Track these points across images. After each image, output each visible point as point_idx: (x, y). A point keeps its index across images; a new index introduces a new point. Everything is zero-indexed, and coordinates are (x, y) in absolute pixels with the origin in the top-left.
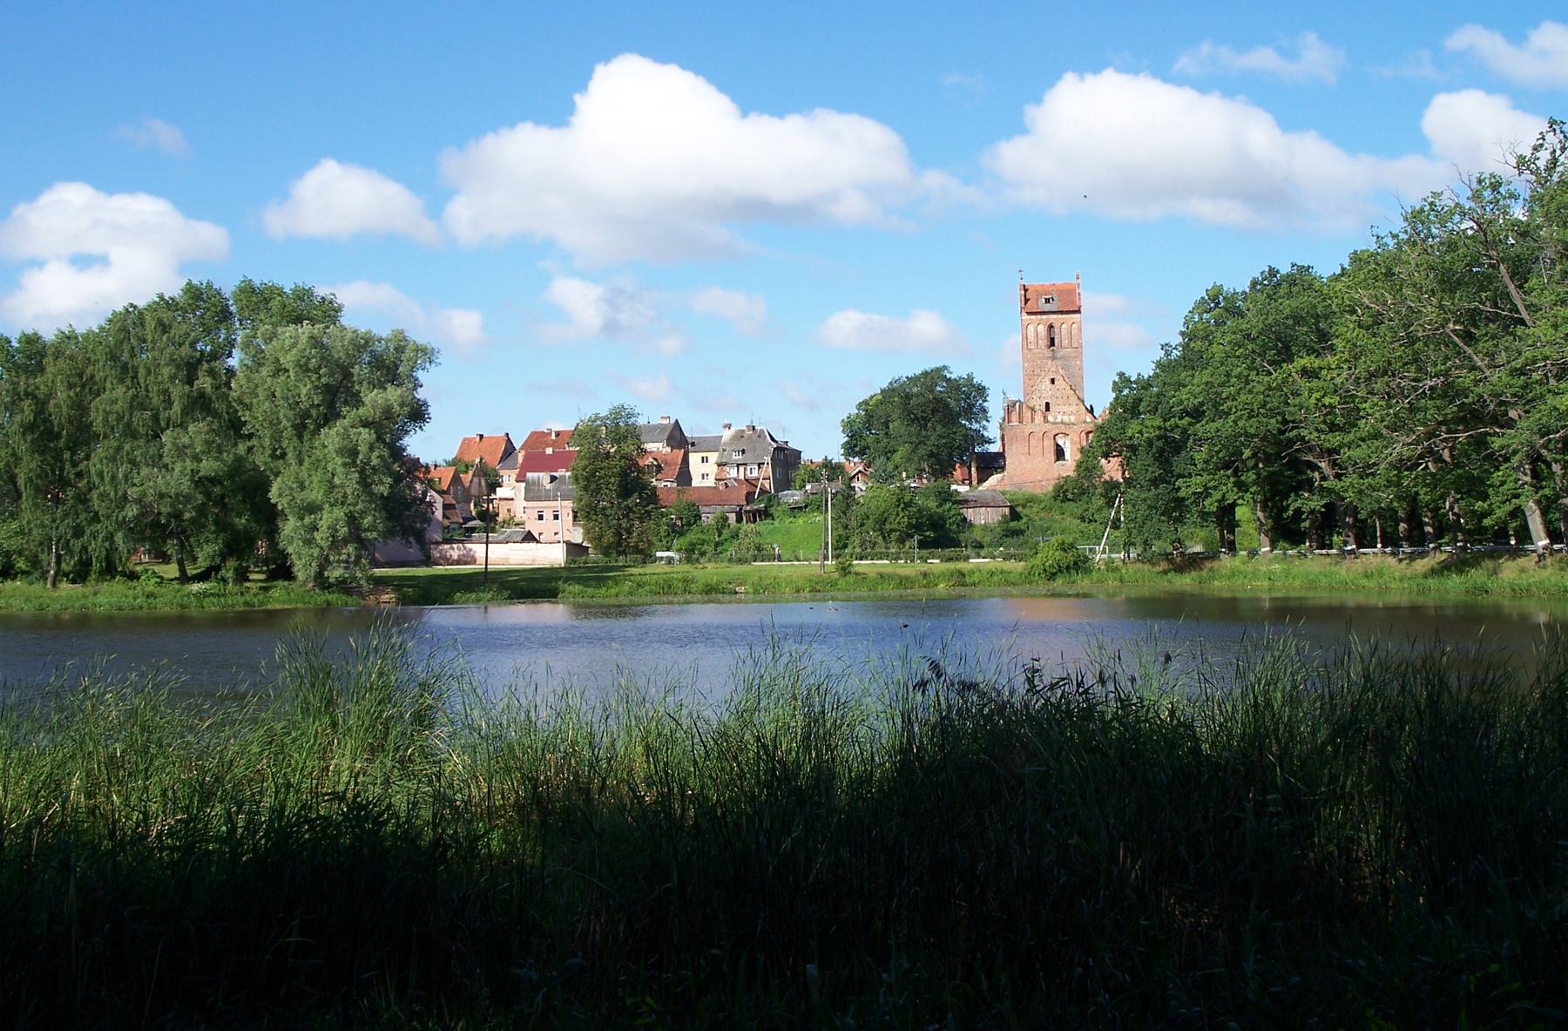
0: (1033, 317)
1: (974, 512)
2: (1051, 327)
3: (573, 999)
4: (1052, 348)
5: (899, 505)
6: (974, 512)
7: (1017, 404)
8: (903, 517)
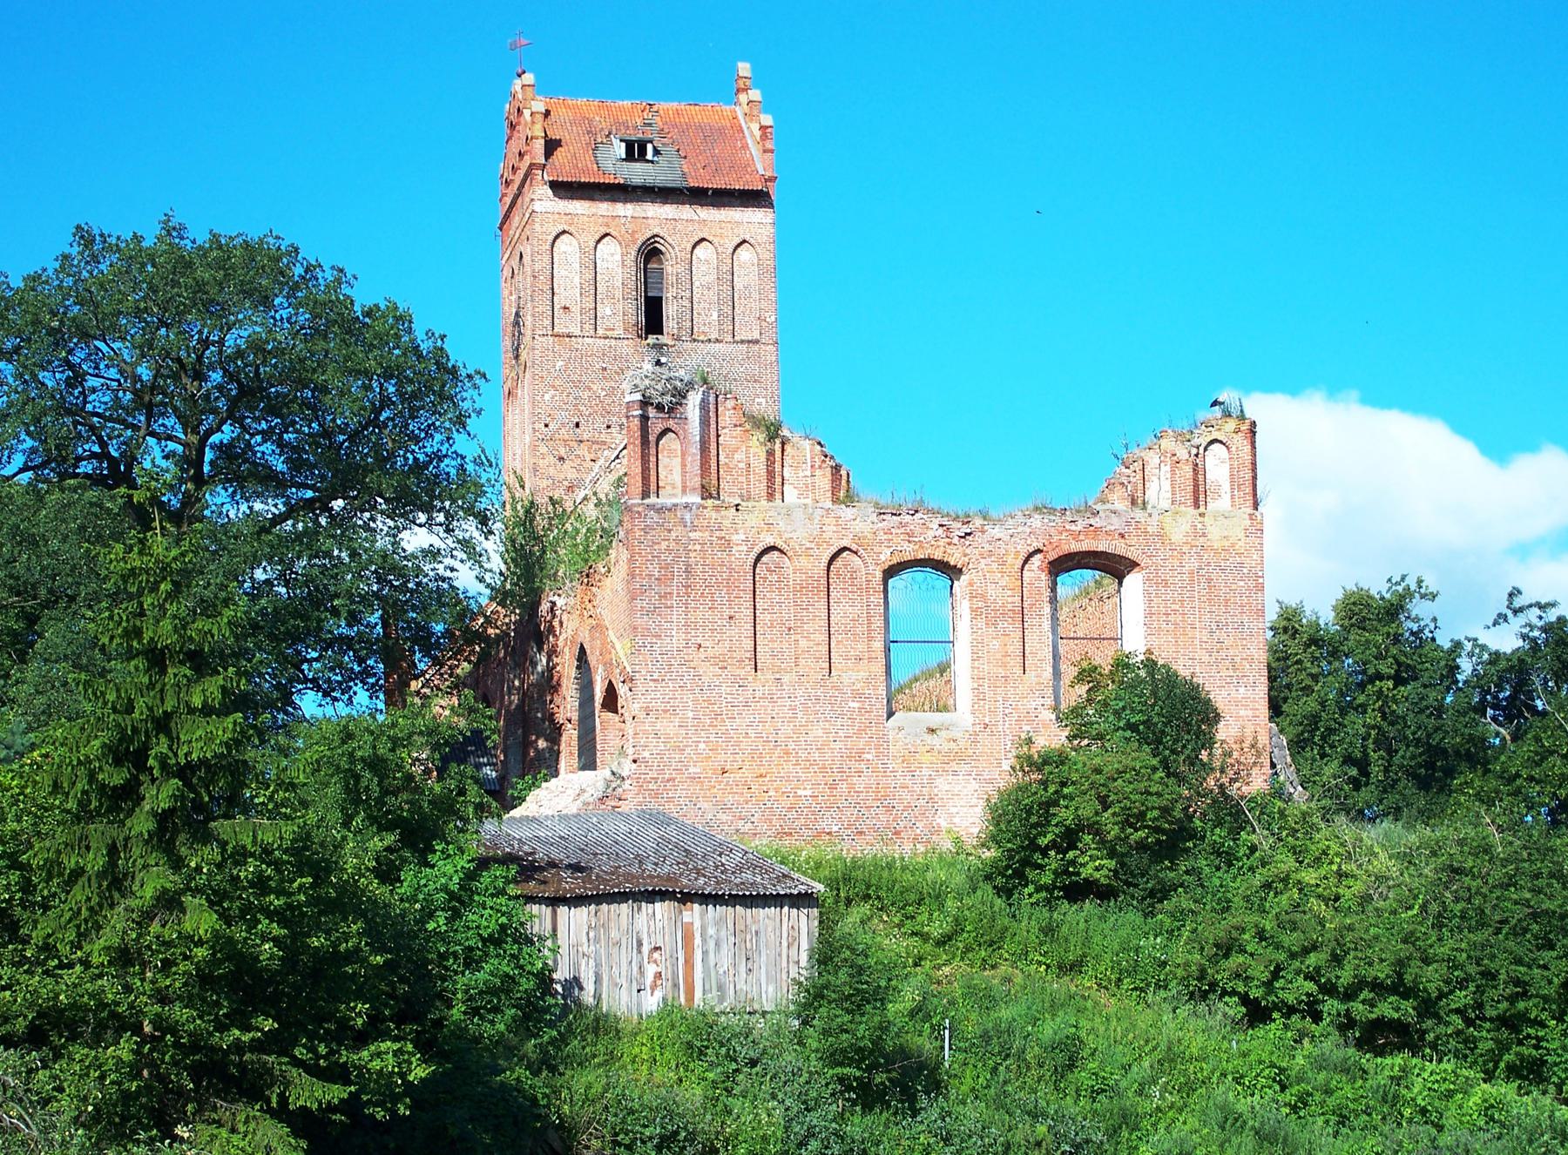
0: (579, 207)
1: (596, 931)
2: (651, 253)
3: (367, 320)
4: (652, 339)
5: (128, 795)
6: (596, 931)
7: (694, 399)
8: (169, 902)
